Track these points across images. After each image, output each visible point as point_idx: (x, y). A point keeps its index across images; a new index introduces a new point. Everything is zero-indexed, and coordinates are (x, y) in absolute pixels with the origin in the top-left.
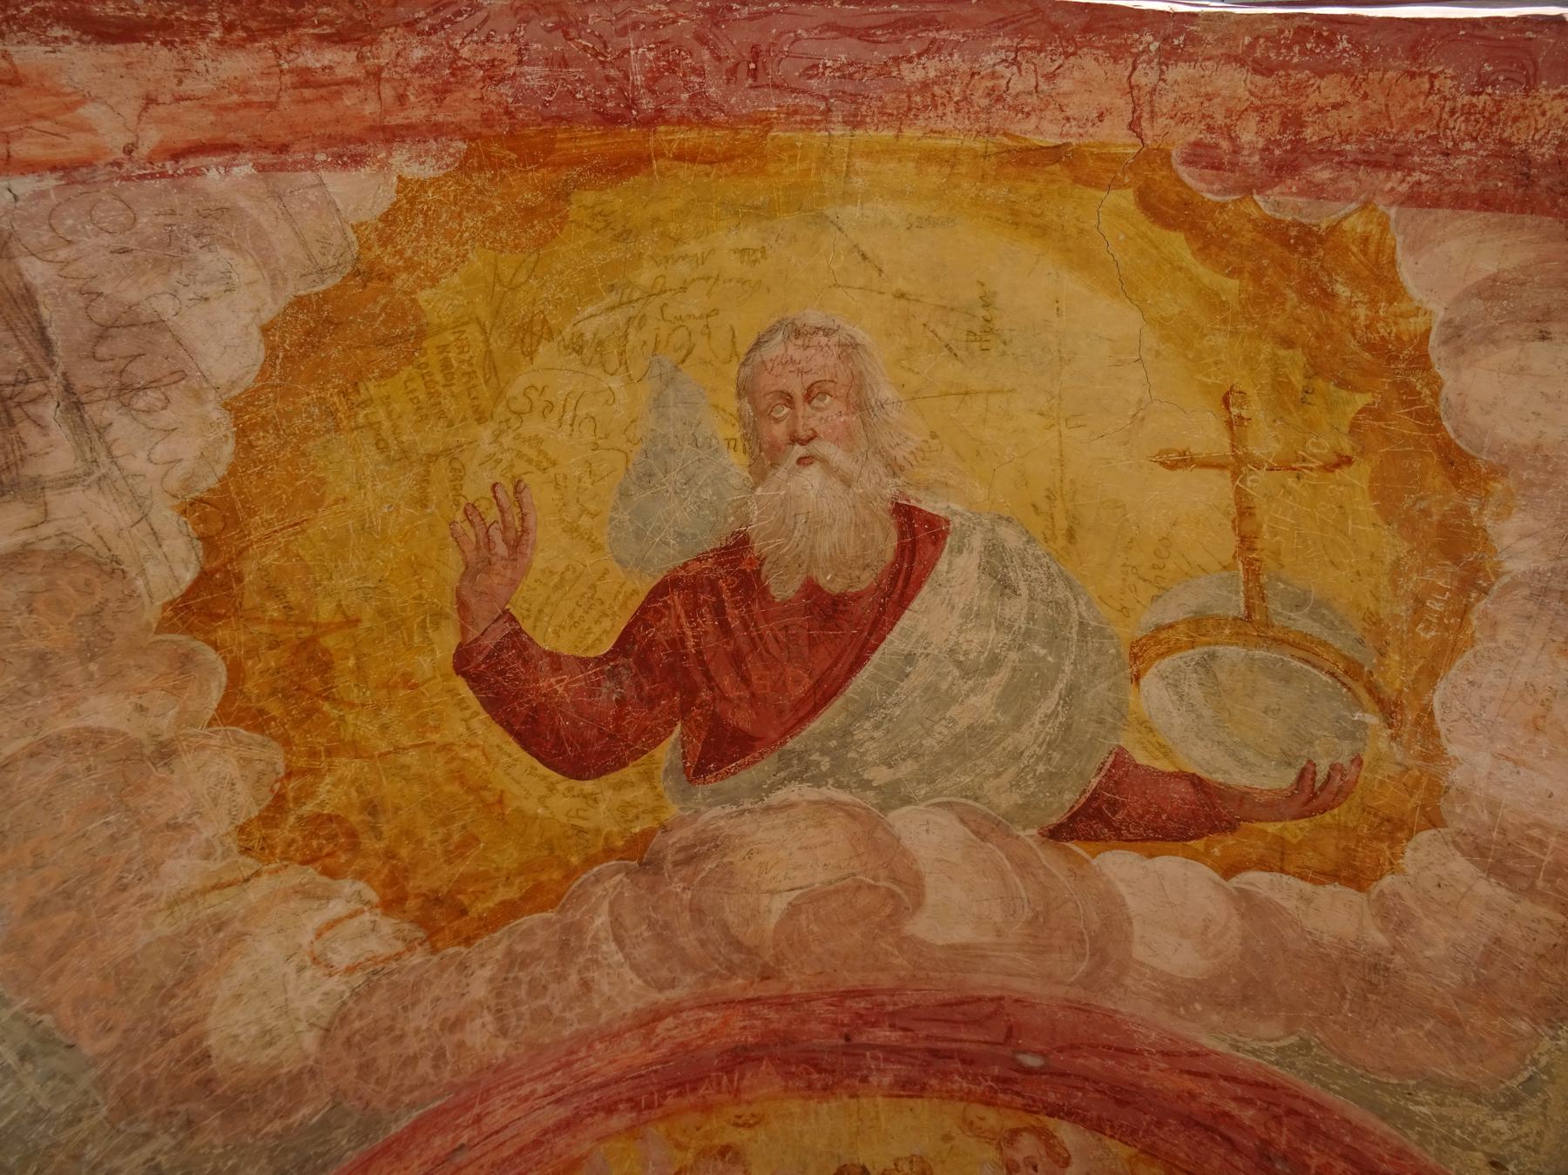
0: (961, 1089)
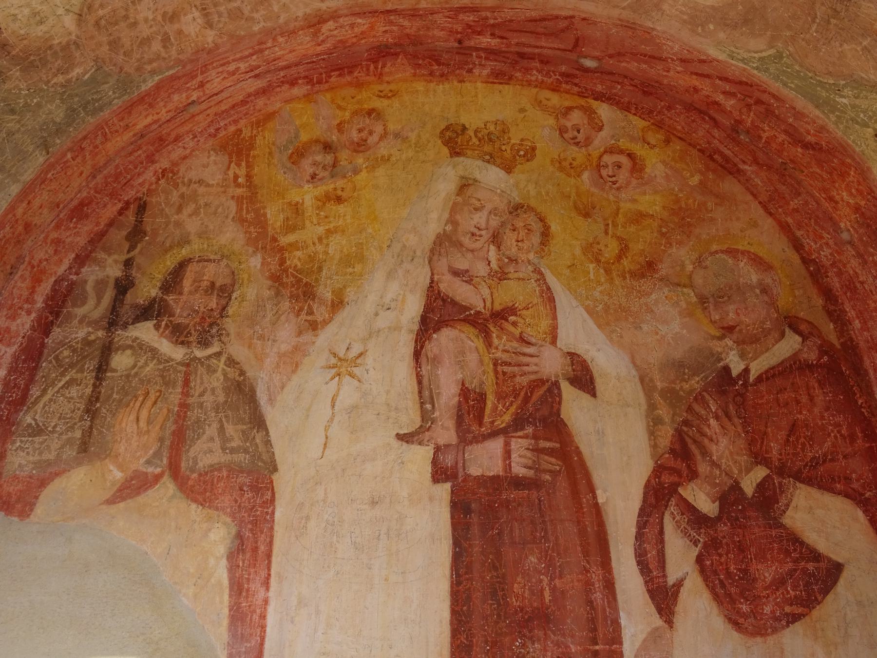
0: (536, 80)
